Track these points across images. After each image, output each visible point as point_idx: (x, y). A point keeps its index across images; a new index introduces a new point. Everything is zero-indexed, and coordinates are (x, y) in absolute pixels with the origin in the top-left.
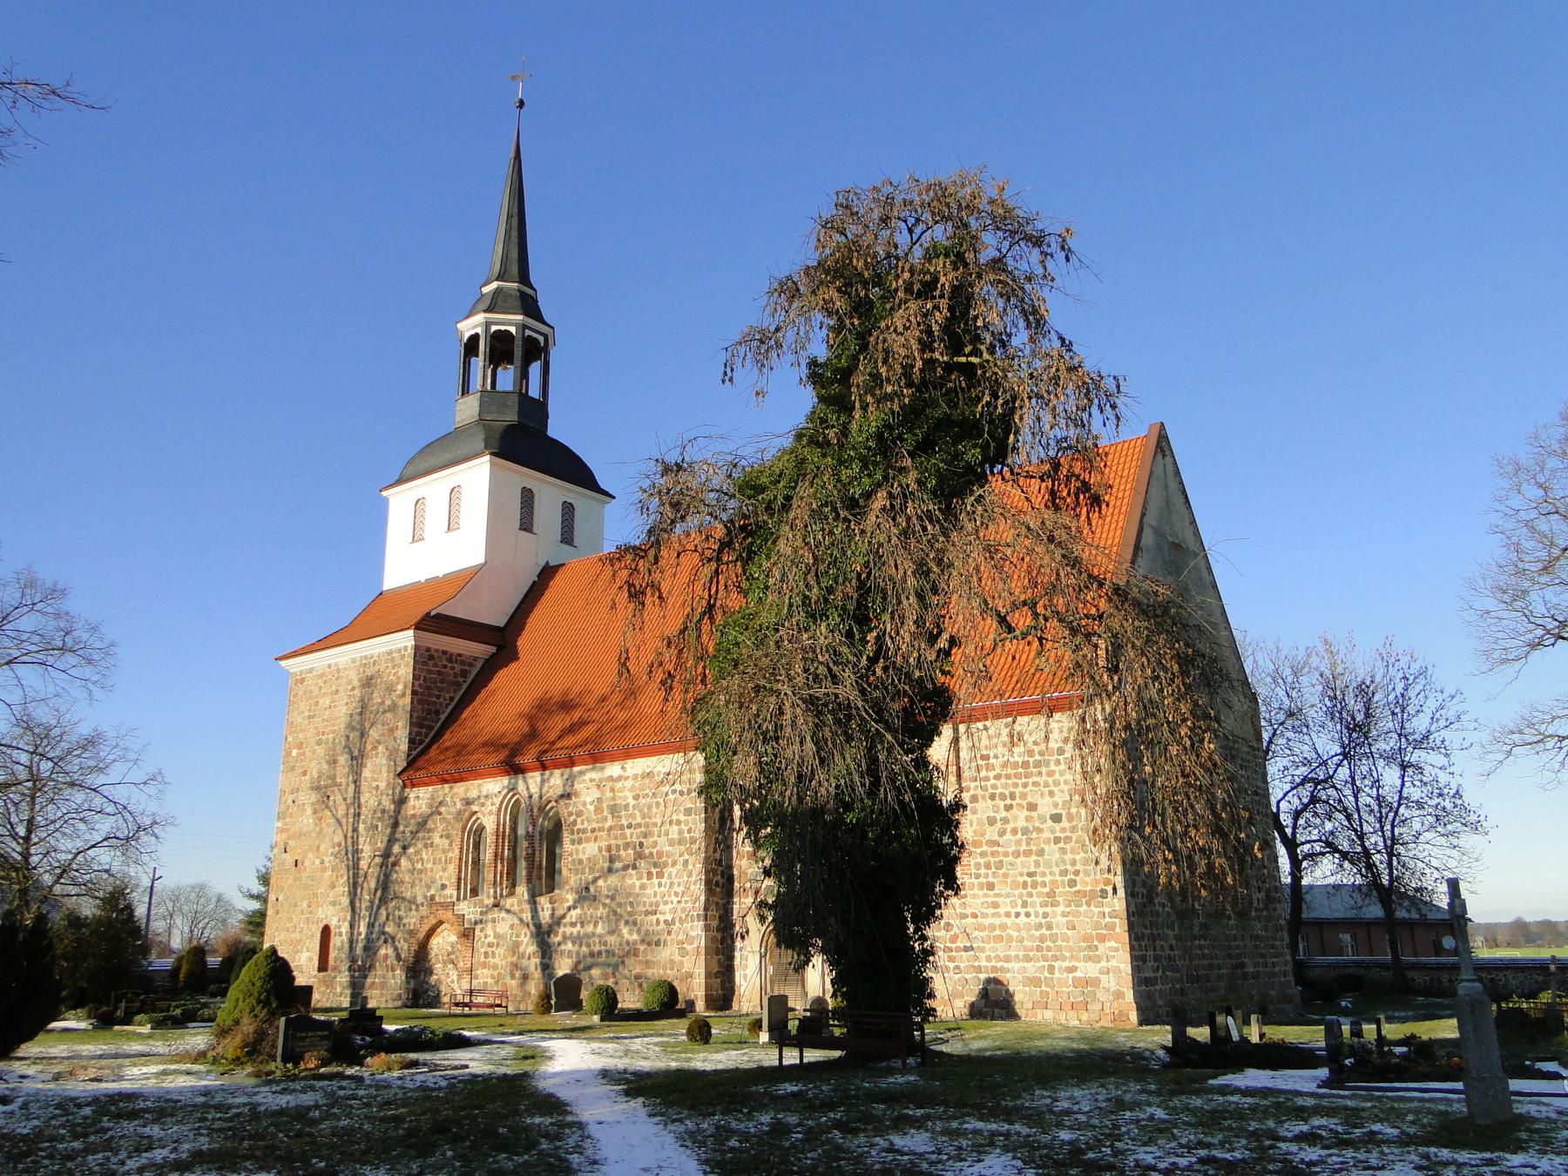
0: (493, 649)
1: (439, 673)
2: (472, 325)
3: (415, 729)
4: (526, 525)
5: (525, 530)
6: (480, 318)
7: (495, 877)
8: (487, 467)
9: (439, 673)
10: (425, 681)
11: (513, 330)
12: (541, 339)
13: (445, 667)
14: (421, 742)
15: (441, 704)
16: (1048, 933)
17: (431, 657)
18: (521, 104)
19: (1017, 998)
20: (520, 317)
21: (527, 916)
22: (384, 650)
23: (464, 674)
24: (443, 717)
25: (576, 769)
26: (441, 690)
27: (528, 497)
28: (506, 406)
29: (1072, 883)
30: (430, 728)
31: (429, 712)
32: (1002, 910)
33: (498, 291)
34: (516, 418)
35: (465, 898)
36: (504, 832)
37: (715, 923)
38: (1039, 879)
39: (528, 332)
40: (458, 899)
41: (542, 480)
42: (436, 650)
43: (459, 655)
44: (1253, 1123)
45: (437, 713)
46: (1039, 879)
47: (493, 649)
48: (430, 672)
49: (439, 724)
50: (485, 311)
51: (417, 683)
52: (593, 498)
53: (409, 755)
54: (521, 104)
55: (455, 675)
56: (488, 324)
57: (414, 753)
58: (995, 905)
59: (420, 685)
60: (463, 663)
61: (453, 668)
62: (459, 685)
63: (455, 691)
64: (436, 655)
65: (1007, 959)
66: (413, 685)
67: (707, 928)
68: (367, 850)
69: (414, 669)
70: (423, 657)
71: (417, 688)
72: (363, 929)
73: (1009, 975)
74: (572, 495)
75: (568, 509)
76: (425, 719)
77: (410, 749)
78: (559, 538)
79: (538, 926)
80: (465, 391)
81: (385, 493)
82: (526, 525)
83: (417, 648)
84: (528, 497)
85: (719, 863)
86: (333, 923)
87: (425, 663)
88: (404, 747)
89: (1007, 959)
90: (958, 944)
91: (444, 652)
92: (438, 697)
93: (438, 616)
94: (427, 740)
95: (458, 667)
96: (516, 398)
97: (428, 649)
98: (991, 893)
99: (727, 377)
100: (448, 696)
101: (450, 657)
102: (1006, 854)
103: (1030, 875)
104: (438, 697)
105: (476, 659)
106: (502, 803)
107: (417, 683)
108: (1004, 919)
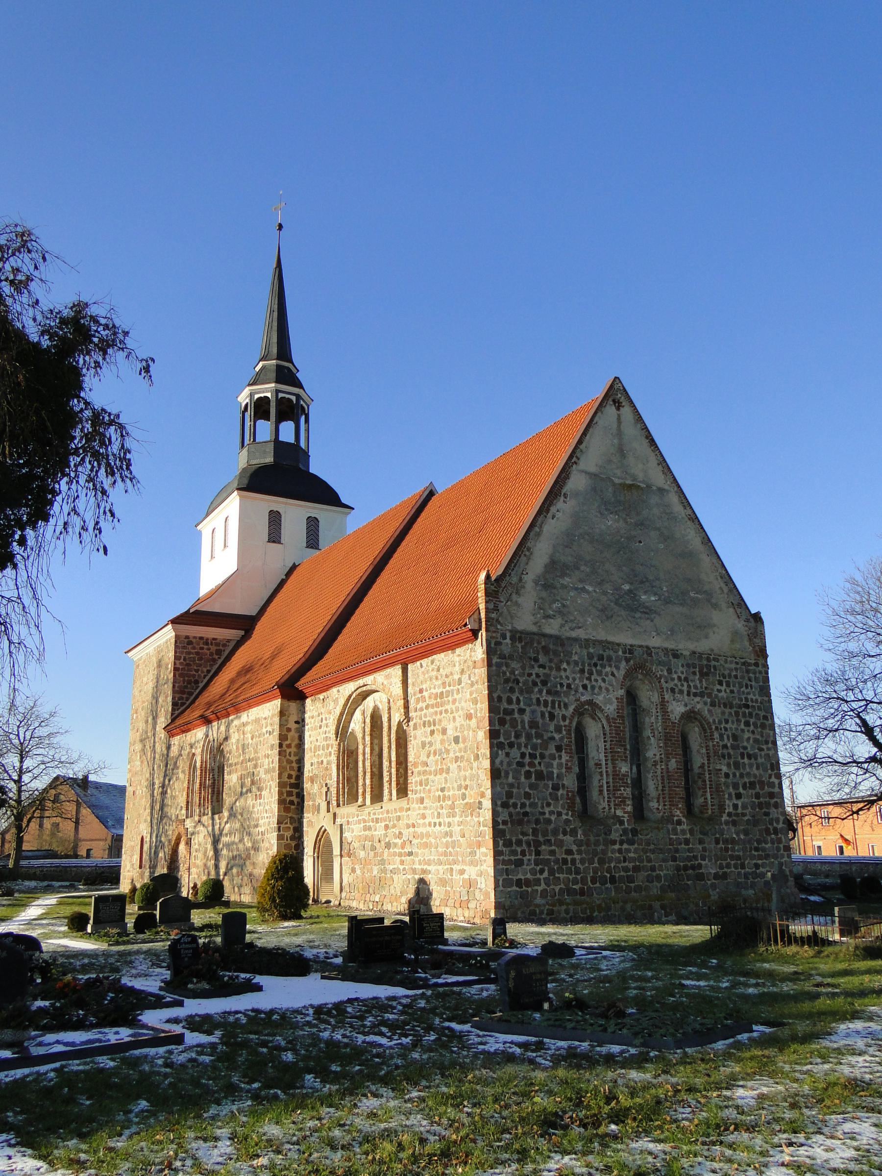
0: (242, 633)
1: (197, 653)
2: (244, 398)
3: (177, 696)
4: (275, 536)
5: (274, 542)
6: (247, 391)
7: (200, 800)
8: (238, 498)
9: (197, 653)
10: (185, 659)
11: (269, 395)
12: (294, 398)
13: (202, 648)
14: (183, 704)
15: (199, 676)
16: (757, 801)
17: (190, 643)
18: (280, 227)
19: (434, 895)
20: (273, 385)
21: (210, 829)
22: (164, 640)
23: (219, 652)
24: (201, 685)
25: (230, 718)
26: (200, 665)
27: (275, 519)
28: (265, 452)
29: (464, 796)
30: (191, 694)
31: (189, 682)
32: (427, 821)
33: (263, 368)
34: (272, 460)
35: (344, 805)
36: (206, 767)
37: (288, 834)
38: (447, 793)
39: (281, 395)
40: (187, 817)
41: (322, 509)
42: (195, 637)
43: (214, 639)
44: (727, 984)
45: (197, 682)
46: (447, 793)
47: (242, 633)
48: (189, 653)
49: (198, 691)
50: (249, 385)
51: (178, 662)
52: (334, 511)
53: (172, 714)
54: (280, 227)
55: (211, 654)
56: (251, 395)
57: (177, 712)
58: (424, 817)
59: (181, 664)
60: (217, 645)
61: (209, 649)
62: (214, 660)
63: (211, 666)
64: (194, 641)
65: (429, 863)
66: (175, 664)
67: (280, 838)
68: (157, 781)
69: (175, 652)
70: (182, 643)
71: (178, 666)
72: (154, 839)
73: (430, 876)
74: (316, 511)
75: (313, 525)
76: (186, 687)
77: (173, 710)
78: (305, 545)
79: (214, 835)
80: (243, 445)
81: (199, 528)
82: (275, 536)
83: (177, 636)
84: (275, 519)
85: (292, 786)
86: (145, 835)
87: (184, 647)
88: (170, 709)
89: (429, 863)
90: (406, 850)
91: (201, 638)
92: (197, 671)
93: (196, 612)
94: (188, 703)
95: (213, 648)
96: (271, 447)
97: (187, 637)
98: (422, 806)
99: (140, 374)
100: (205, 670)
101: (206, 642)
102: (430, 773)
103: (442, 790)
104: (197, 671)
105: (229, 641)
106: (204, 746)
107: (178, 662)
108: (428, 829)
